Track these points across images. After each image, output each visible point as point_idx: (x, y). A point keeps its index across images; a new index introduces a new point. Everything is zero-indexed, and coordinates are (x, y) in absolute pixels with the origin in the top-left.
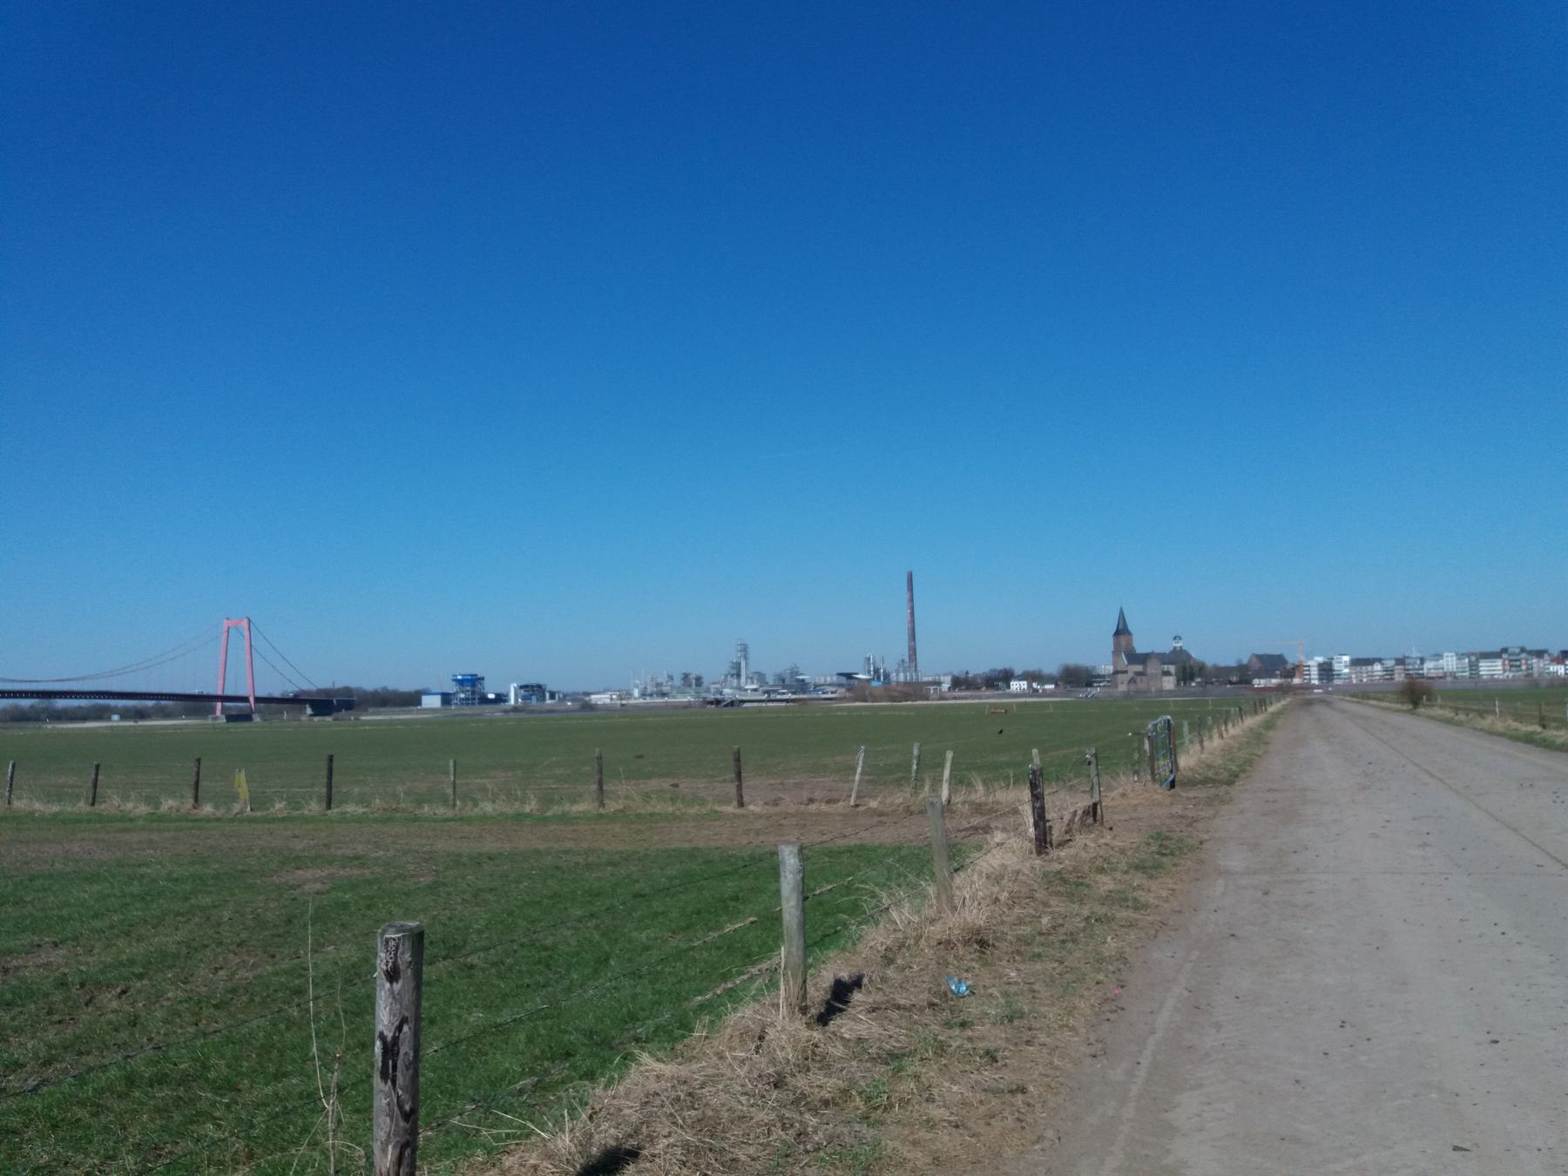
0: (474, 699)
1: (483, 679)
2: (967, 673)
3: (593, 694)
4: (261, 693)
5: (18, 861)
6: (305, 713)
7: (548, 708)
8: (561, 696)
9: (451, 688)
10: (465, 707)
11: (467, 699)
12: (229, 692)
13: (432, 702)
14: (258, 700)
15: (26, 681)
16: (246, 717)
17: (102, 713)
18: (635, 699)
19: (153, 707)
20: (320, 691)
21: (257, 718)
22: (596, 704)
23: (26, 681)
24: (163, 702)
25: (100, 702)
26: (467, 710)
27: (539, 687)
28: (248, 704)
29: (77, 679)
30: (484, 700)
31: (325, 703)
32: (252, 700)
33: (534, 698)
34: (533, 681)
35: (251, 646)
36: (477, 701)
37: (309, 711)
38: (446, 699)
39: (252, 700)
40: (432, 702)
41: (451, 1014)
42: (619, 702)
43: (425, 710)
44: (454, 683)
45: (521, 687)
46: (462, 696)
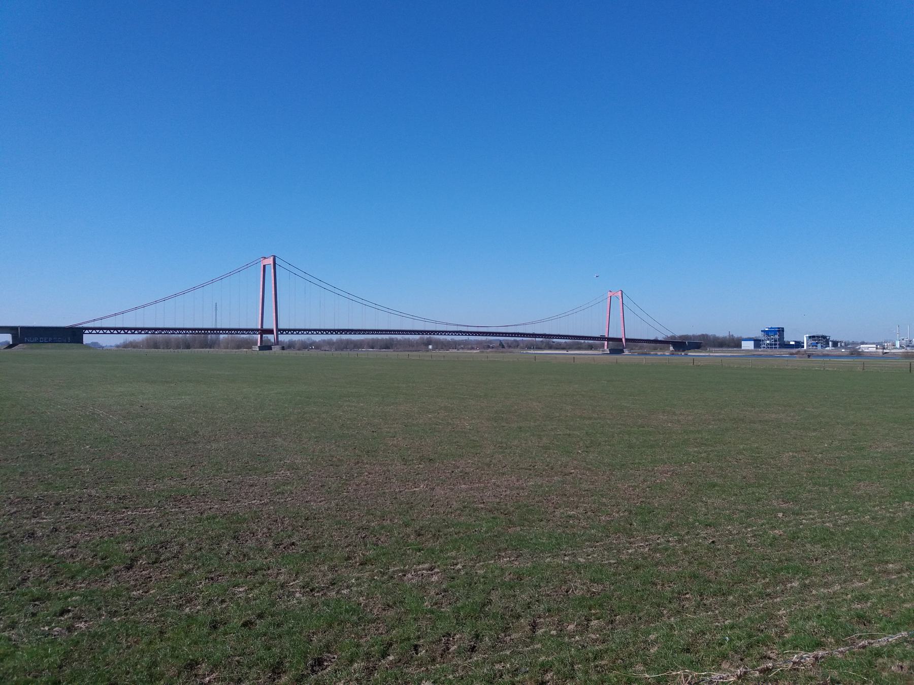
0: (775, 344)
1: (783, 328)
2: (126, 340)
3: (863, 343)
4: (628, 337)
5: (495, 431)
6: (669, 350)
7: (826, 353)
8: (843, 344)
9: (760, 335)
10: (769, 350)
11: (771, 344)
12: (219, 327)
13: (748, 345)
14: (627, 340)
15: (216, 319)
16: (620, 351)
17: (516, 345)
18: (896, 348)
19: (143, 341)
20: (680, 337)
21: (626, 352)
22: (863, 352)
23: (216, 319)
24: (537, 339)
25: (548, 340)
26: (769, 351)
27: (824, 337)
28: (621, 343)
29: (541, 321)
30: (787, 346)
31: (681, 344)
32: (624, 340)
33: (819, 345)
34: (820, 334)
35: (623, 303)
36: (777, 346)
37: (671, 348)
38: (757, 343)
39: (624, 340)
40: (748, 345)
41: (541, 681)
42: (881, 351)
43: (743, 350)
44: (763, 333)
45: (810, 337)
46: (768, 342)
